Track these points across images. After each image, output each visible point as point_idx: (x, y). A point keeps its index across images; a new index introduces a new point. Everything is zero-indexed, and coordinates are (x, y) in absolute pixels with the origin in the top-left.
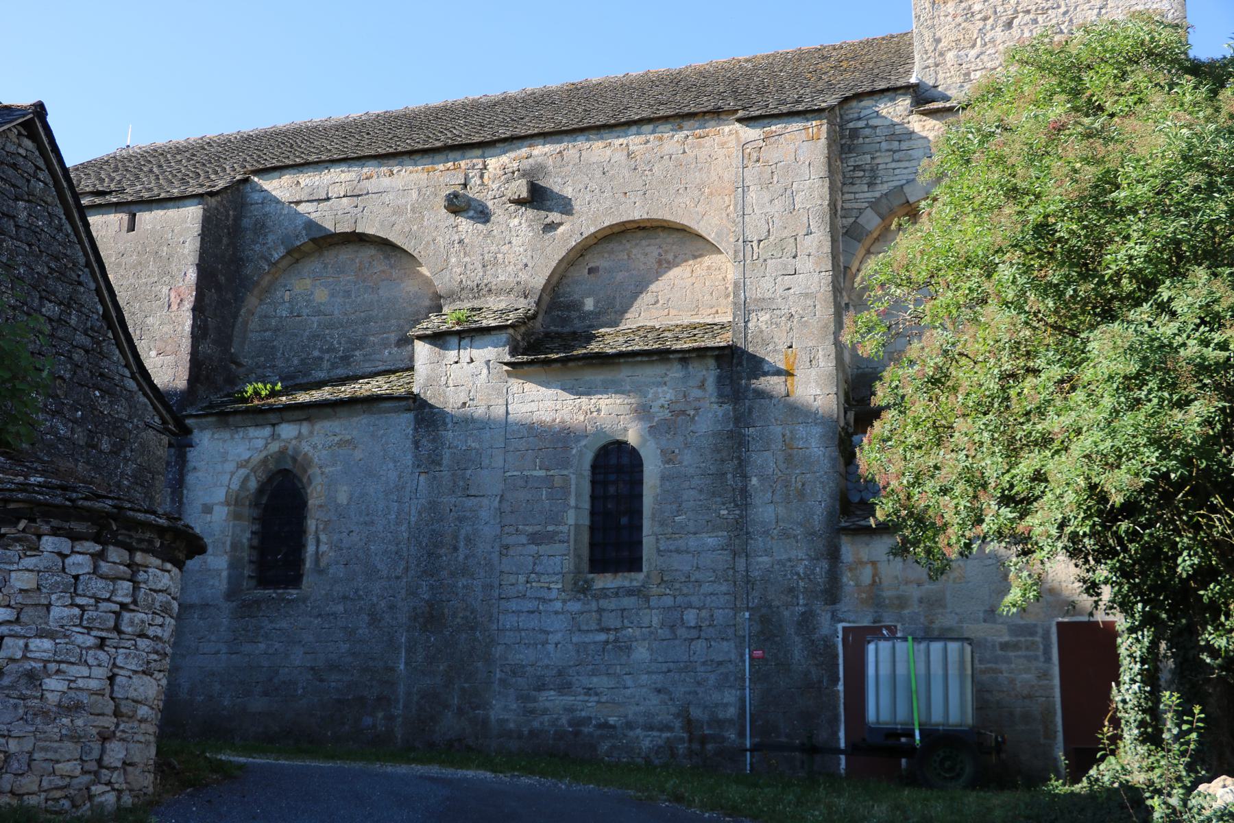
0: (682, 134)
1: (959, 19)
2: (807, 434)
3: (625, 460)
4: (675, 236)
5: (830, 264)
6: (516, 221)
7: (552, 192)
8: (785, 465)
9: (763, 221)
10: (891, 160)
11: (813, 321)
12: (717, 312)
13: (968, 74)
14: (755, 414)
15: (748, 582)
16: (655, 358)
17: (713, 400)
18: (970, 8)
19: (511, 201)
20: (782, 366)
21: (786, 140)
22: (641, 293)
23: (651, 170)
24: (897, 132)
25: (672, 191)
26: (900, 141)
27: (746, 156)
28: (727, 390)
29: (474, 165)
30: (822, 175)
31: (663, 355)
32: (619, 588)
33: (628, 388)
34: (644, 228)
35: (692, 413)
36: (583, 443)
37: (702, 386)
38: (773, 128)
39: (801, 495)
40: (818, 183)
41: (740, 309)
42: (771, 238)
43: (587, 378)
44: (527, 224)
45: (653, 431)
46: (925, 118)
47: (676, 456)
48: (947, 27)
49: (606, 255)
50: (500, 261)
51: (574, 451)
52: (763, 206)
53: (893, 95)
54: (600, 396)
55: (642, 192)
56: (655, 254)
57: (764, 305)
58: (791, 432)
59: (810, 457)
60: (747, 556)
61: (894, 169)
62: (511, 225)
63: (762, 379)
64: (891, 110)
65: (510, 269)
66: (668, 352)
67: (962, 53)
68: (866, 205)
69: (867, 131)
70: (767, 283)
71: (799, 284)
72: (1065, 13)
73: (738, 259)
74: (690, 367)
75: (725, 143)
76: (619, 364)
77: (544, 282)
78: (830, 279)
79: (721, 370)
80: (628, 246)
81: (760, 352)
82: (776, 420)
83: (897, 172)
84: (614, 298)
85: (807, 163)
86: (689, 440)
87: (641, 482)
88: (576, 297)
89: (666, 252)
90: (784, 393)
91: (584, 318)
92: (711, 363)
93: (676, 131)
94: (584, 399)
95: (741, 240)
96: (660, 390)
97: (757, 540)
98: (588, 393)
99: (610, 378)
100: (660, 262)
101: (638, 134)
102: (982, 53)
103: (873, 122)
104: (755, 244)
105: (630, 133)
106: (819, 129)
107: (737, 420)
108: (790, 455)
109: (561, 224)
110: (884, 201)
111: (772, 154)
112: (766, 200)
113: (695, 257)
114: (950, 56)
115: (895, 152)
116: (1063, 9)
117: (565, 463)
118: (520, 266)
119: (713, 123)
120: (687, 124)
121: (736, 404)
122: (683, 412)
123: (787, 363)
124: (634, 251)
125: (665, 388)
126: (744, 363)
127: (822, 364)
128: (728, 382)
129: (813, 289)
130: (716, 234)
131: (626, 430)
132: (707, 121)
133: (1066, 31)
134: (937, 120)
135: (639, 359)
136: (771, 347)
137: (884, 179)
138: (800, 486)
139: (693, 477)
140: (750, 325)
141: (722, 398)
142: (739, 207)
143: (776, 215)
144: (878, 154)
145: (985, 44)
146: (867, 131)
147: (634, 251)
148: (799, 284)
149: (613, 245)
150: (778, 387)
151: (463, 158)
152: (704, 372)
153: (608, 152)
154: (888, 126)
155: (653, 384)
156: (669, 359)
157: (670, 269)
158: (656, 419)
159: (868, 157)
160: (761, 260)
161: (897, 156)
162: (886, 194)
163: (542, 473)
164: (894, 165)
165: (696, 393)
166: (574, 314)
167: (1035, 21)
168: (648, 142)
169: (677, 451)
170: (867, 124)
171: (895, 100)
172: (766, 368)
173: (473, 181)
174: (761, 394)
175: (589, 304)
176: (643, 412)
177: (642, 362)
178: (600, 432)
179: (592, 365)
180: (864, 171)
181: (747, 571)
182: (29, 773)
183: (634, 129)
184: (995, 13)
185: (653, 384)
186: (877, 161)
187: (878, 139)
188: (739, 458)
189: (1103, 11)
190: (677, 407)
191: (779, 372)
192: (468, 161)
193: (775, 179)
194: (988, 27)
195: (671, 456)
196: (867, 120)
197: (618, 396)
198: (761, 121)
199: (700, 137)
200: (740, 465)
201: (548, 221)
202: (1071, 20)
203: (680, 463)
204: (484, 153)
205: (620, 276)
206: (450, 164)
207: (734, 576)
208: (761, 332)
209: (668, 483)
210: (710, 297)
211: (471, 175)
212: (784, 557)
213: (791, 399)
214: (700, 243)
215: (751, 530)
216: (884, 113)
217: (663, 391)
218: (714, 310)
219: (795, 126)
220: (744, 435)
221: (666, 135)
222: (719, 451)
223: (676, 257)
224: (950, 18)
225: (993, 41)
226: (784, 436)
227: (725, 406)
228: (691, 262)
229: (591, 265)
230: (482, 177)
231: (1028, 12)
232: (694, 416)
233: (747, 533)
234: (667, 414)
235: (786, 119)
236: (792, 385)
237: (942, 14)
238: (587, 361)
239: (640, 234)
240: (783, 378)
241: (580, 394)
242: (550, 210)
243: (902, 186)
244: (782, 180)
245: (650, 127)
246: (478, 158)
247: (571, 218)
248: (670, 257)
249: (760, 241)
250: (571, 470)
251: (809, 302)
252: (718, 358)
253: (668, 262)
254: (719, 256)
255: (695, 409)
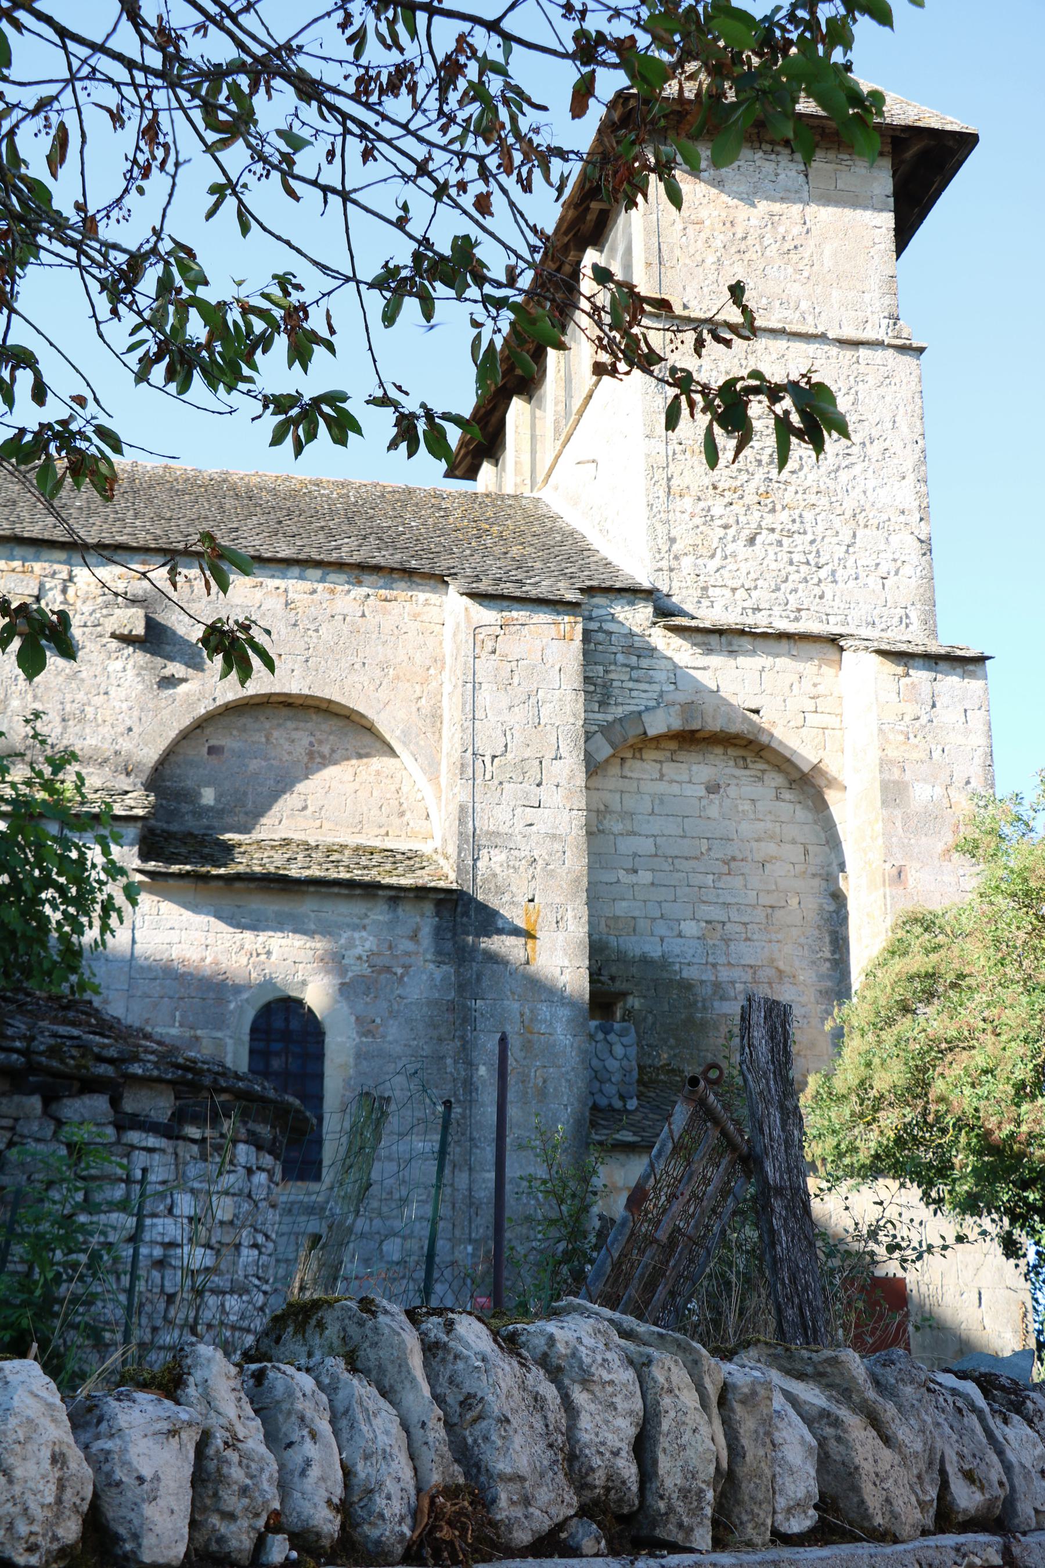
0: (364, 590)
1: (698, 521)
2: (552, 1016)
3: (295, 1025)
4: (334, 723)
5: (584, 802)
6: (118, 665)
7: (174, 633)
8: (523, 1054)
9: (499, 732)
10: (627, 677)
11: (562, 871)
12: (387, 834)
13: (705, 589)
14: (485, 983)
15: (471, 1205)
16: (358, 892)
17: (429, 957)
18: (709, 510)
19: (113, 635)
20: (521, 923)
21: (530, 632)
22: (284, 793)
23: (317, 631)
24: (637, 645)
25: (344, 664)
26: (639, 656)
27: (478, 643)
28: (448, 946)
29: (55, 573)
30: (576, 686)
31: (370, 890)
32: (293, 1203)
33: (313, 927)
34: (290, 705)
35: (400, 971)
36: (245, 996)
37: (414, 937)
38: (514, 614)
39: (542, 1094)
40: (570, 696)
41: (467, 842)
42: (510, 756)
43: (254, 906)
44: (135, 672)
45: (346, 990)
46: (670, 634)
47: (377, 1027)
48: (684, 526)
49: (235, 732)
50: (90, 716)
51: (232, 1006)
52: (500, 712)
53: (632, 597)
54: (271, 933)
55: (303, 658)
56: (305, 742)
57: (499, 841)
58: (532, 1011)
59: (554, 1046)
60: (470, 1169)
61: (631, 690)
62: (110, 669)
63: (496, 937)
64: (629, 615)
65: (104, 730)
66: (378, 886)
67: (700, 561)
68: (596, 728)
69: (601, 636)
70: (502, 814)
71: (545, 820)
72: (812, 542)
73: (465, 776)
74: (400, 910)
75: (419, 614)
76: (304, 893)
77: (156, 757)
78: (583, 820)
79: (441, 918)
80: (267, 725)
81: (493, 902)
82: (513, 993)
83: (634, 694)
84: (245, 794)
85: (557, 668)
86: (396, 1007)
87: (320, 1057)
88: (189, 783)
89: (320, 742)
90: (523, 960)
91: (200, 815)
92: (429, 908)
93: (353, 585)
94: (248, 935)
95: (470, 751)
96: (356, 935)
97: (484, 1149)
98: (255, 927)
99: (286, 909)
100: (311, 755)
101: (301, 578)
102: (723, 567)
103: (607, 626)
104: (488, 760)
105: (289, 574)
106: (573, 628)
107: (461, 987)
108: (529, 1041)
109: (185, 680)
110: (618, 726)
111: (512, 645)
112: (505, 704)
113: (360, 756)
114: (687, 562)
115: (633, 668)
116: (809, 537)
117: (219, 1022)
118: (121, 729)
119: (403, 585)
120: (368, 579)
121: (460, 966)
122: (388, 969)
123: (528, 921)
124: (276, 734)
125: (364, 934)
126: (472, 913)
127: (571, 928)
128: (449, 935)
129: (561, 831)
130: (403, 732)
131: (304, 983)
132: (394, 581)
133: (812, 563)
134: (685, 639)
135: (336, 890)
136: (506, 898)
137: (620, 700)
138: (540, 1081)
139: (400, 1058)
140: (479, 864)
141: (441, 956)
142: (469, 707)
143: (517, 726)
144: (612, 667)
145: (726, 558)
146: (601, 636)
147: (276, 734)
148: (545, 820)
149: (246, 720)
150: (516, 950)
151: (37, 559)
152: (418, 919)
153: (259, 594)
154: (625, 635)
155: (348, 925)
156: (375, 896)
157: (324, 766)
158: (350, 974)
159: (601, 668)
160: (496, 782)
161: (635, 674)
162: (620, 719)
163: (199, 1032)
164: (631, 685)
165: (407, 945)
166: (185, 808)
167: (780, 543)
168: (314, 592)
169: (378, 1020)
170: (601, 627)
171: (634, 604)
172: (500, 924)
173: (50, 594)
174: (492, 958)
175: (208, 796)
176: (335, 962)
177: (338, 895)
178: (268, 983)
179: (267, 890)
180: (595, 685)
181: (470, 1190)
182: (292, 1521)
183: (296, 571)
184: (738, 522)
185: (348, 925)
186: (612, 676)
187: (614, 649)
188: (462, 1038)
189: (851, 550)
190: (379, 961)
191: (516, 932)
192: (46, 565)
193: (516, 681)
194: (730, 538)
195: (372, 1026)
196: (601, 622)
197: (297, 936)
198: (499, 602)
199: (385, 600)
200: (464, 1047)
201: (167, 672)
202: (818, 552)
203: (383, 1037)
204: (70, 558)
205: (254, 765)
206: (17, 564)
207: (452, 1195)
208: (495, 875)
209: (365, 1063)
210: (378, 813)
211: (48, 586)
212: (518, 1174)
213: (532, 968)
214: (368, 739)
215: (476, 1135)
216: (621, 617)
217: (361, 938)
218: (383, 831)
219: (542, 617)
220: (470, 1009)
221: (339, 588)
222: (436, 1027)
223: (333, 751)
224: (686, 516)
225: (734, 555)
226: (522, 1015)
227: (445, 967)
228: (354, 762)
229: (212, 742)
230: (64, 591)
231: (773, 530)
232: (402, 976)
233: (472, 1139)
234: (365, 969)
235: (530, 606)
236: (533, 949)
237: (678, 509)
238: (263, 884)
239: (285, 712)
240: (522, 940)
241: (243, 927)
242: (171, 659)
243: (640, 713)
244: (524, 684)
245: (318, 573)
246: (60, 562)
247: (200, 674)
248: (326, 750)
249: (494, 757)
250: (228, 1033)
251: (557, 846)
252: (439, 904)
253: (323, 757)
254: (393, 760)
255: (404, 966)
